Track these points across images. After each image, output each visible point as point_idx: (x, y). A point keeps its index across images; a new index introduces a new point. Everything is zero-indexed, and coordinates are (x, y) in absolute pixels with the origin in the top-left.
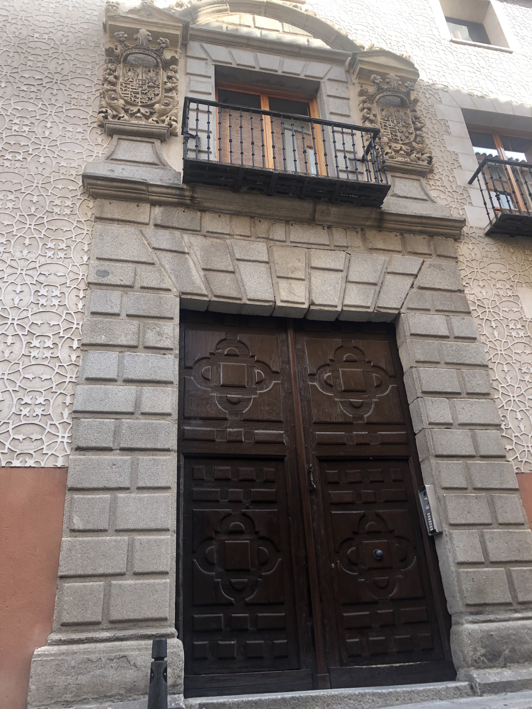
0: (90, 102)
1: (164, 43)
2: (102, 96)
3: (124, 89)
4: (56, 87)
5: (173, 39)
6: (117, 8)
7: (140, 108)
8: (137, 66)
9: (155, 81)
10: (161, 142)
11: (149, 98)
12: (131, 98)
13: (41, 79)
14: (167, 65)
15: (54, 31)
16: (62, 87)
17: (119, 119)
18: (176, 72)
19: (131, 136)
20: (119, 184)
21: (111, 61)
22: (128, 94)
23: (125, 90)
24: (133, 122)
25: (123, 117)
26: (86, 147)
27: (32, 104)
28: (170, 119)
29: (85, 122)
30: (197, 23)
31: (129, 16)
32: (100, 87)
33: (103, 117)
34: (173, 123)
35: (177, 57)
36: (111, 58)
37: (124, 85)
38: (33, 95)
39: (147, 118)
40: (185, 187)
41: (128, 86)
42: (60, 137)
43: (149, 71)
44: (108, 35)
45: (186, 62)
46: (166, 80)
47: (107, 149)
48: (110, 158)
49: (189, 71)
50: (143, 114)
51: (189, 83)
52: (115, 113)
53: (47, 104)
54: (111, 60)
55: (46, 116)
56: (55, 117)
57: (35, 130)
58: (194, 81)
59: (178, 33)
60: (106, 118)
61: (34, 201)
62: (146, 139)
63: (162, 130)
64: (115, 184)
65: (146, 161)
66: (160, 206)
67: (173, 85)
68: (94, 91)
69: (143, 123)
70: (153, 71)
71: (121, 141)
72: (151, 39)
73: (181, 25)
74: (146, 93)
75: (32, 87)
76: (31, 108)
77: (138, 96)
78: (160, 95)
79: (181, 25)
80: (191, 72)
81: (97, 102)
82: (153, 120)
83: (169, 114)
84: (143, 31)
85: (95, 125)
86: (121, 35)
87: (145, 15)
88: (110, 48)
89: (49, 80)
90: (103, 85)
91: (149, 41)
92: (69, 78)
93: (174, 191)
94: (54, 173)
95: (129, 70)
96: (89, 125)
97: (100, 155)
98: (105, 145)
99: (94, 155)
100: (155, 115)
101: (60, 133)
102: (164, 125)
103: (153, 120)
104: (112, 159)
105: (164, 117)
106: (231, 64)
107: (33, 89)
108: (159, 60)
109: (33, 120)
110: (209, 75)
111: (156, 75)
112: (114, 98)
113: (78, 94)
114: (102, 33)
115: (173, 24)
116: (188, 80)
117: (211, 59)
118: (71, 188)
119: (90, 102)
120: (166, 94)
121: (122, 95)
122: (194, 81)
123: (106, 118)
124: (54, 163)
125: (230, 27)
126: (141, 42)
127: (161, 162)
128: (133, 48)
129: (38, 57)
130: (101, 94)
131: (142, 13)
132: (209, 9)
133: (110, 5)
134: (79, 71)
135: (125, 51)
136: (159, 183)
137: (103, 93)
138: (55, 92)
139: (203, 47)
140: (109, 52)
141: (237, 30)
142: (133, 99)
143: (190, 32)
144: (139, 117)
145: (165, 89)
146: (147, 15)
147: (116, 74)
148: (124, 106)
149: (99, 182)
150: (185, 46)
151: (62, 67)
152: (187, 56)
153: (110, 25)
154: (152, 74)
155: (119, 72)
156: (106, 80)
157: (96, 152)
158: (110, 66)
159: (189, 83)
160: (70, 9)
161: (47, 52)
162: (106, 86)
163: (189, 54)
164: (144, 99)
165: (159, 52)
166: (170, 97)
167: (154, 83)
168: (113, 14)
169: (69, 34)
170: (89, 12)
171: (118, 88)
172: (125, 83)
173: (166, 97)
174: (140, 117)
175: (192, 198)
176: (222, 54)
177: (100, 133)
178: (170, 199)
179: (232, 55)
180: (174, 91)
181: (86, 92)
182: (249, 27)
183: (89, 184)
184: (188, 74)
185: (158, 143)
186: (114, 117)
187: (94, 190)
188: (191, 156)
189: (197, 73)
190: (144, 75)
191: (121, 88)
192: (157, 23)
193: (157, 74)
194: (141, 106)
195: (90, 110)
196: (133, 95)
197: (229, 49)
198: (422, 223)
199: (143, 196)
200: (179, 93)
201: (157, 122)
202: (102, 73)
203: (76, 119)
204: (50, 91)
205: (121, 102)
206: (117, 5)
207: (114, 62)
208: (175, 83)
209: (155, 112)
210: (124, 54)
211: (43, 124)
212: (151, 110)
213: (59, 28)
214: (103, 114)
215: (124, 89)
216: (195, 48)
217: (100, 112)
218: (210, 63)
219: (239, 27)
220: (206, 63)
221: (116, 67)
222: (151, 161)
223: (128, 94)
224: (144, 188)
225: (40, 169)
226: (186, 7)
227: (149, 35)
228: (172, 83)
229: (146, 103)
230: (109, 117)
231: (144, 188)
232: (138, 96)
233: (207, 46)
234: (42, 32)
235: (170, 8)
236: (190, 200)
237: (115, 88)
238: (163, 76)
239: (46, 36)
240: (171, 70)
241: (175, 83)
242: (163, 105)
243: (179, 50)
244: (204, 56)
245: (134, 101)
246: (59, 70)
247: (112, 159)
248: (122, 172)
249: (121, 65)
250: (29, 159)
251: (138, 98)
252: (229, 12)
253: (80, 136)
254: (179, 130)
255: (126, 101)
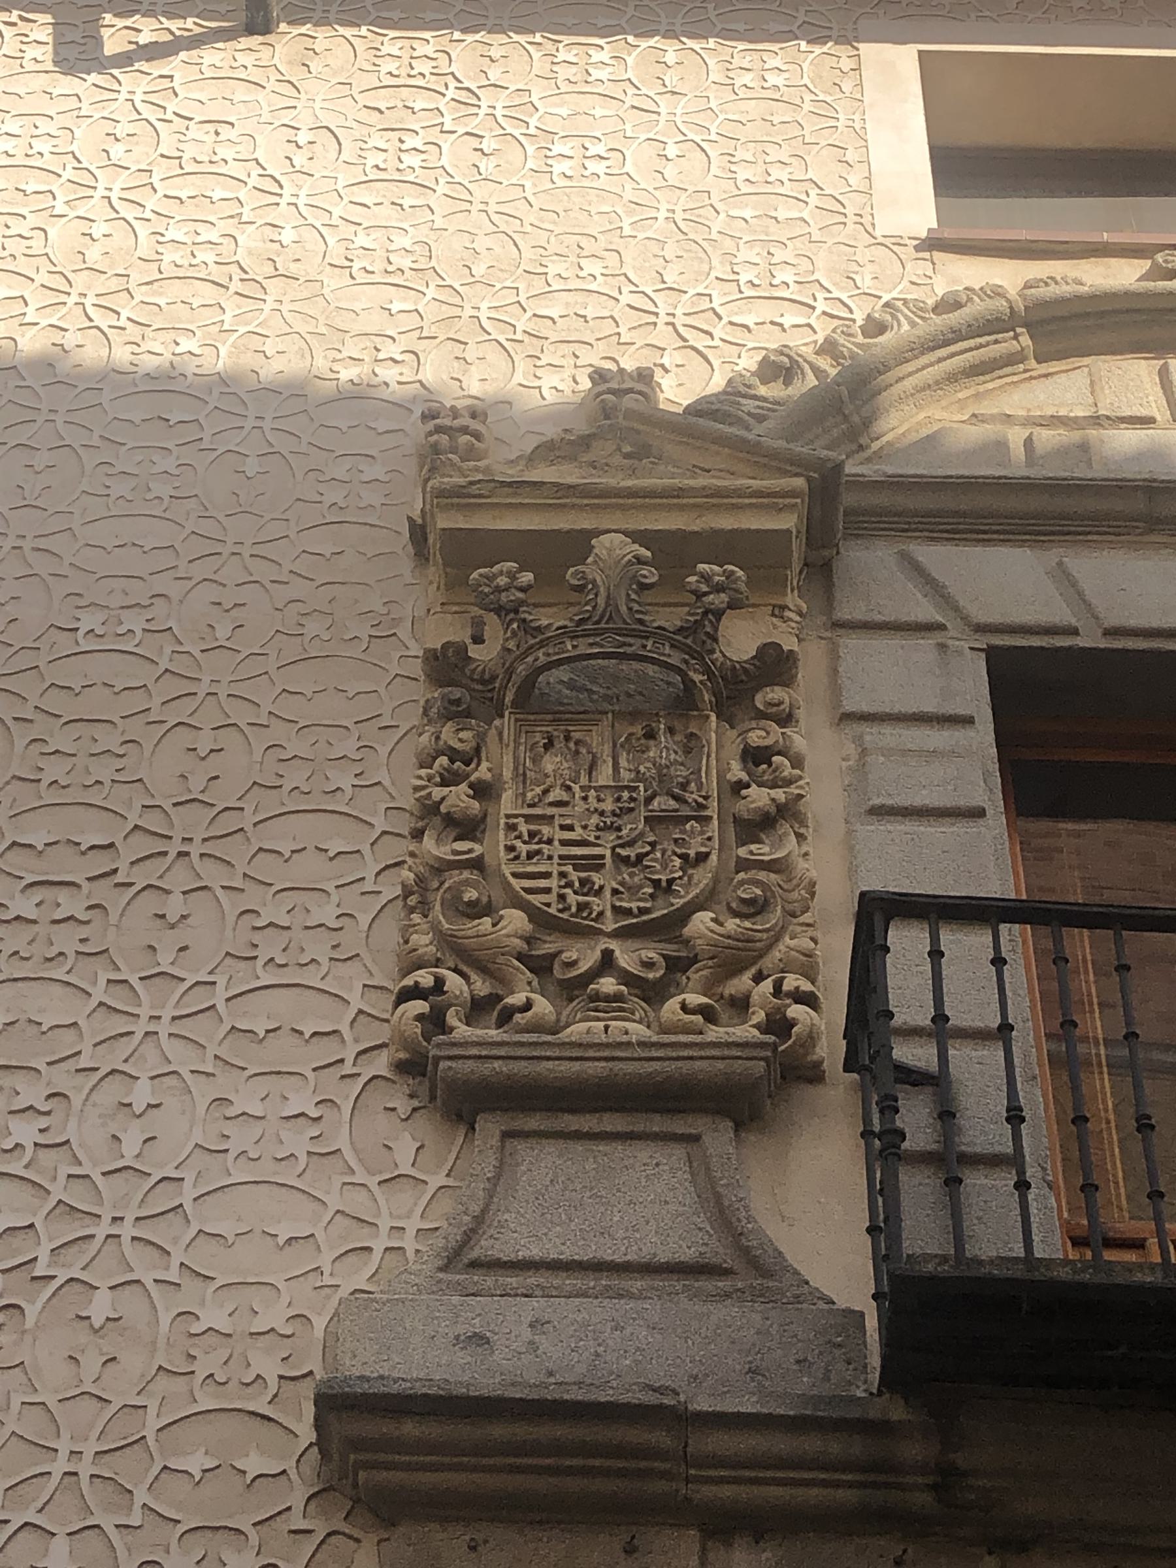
0: (352, 941)
1: (719, 589)
2: (412, 900)
3: (523, 849)
4: (179, 878)
5: (759, 556)
6: (477, 436)
7: (613, 945)
8: (588, 717)
9: (684, 786)
10: (738, 1126)
11: (656, 883)
12: (562, 897)
13: (111, 845)
14: (745, 688)
15: (175, 590)
16: (212, 874)
17: (506, 1017)
18: (786, 719)
19: (572, 1111)
20: (522, 1431)
21: (454, 712)
22: (546, 875)
23: (530, 856)
24: (576, 1031)
25: (528, 1006)
26: (334, 1202)
27: (57, 989)
28: (777, 990)
29: (326, 1051)
30: (875, 446)
31: (534, 476)
32: (398, 848)
33: (420, 1018)
34: (796, 1011)
35: (789, 643)
36: (457, 693)
37: (524, 828)
38: (67, 940)
39: (653, 993)
40: (898, 1412)
41: (546, 830)
42: (199, 1157)
43: (651, 735)
44: (434, 572)
45: (834, 655)
46: (737, 772)
47: (446, 1204)
48: (465, 1259)
49: (854, 702)
50: (627, 978)
51: (861, 768)
52: (482, 987)
53: (134, 981)
54: (458, 702)
55: (125, 1047)
56: (172, 1048)
57: (71, 1132)
58: (887, 752)
59: (787, 522)
60: (435, 1022)
61: (172, 918)
62: (657, 1123)
63: (739, 1066)
64: (499, 1431)
65: (663, 1257)
66: (758, 1536)
67: (780, 794)
68: (370, 876)
69: (638, 1031)
70: (671, 730)
71: (520, 1146)
72: (650, 575)
73: (800, 483)
74: (640, 857)
75: (63, 895)
76: (53, 1006)
77: (597, 879)
78: (714, 857)
79: (800, 483)
80: (865, 708)
81: (389, 935)
82: (684, 1007)
83: (767, 963)
84: (613, 545)
85: (381, 1064)
86: (502, 581)
87: (617, 460)
88: (445, 646)
89: (143, 845)
90: (417, 835)
91: (644, 587)
92: (247, 820)
93: (835, 1447)
94: (163, 1381)
95: (549, 746)
96: (348, 1069)
97: (409, 1243)
98: (438, 1179)
99: (378, 1246)
100: (696, 975)
101: (197, 1137)
102: (746, 1032)
103: (684, 1007)
104: (474, 1265)
105: (744, 981)
106: (1075, 632)
107: (70, 904)
108: (697, 678)
109: (61, 1079)
110: (961, 711)
111: (688, 751)
112: (471, 904)
113: (290, 899)
114: (405, 566)
115: (756, 484)
116: (851, 749)
117: (965, 619)
118: (254, 1464)
119: (352, 941)
120: (742, 852)
121: (517, 884)
122: (887, 752)
123: (435, 1022)
124: (165, 1319)
125: (1047, 438)
126: (601, 601)
127: (745, 1252)
128: (565, 633)
129: (98, 731)
130: (407, 893)
131: (601, 450)
132: (932, 367)
133: (439, 430)
134: (295, 777)
135: (526, 654)
136: (748, 1405)
137: (420, 880)
138: (174, 906)
139: (918, 571)
140: (445, 665)
141: (1084, 447)
142: (573, 899)
143: (848, 499)
144: (608, 999)
145: (736, 820)
146: (627, 456)
147: (483, 772)
148: (529, 940)
149: (410, 1429)
150: (821, 572)
151: (214, 765)
152: (838, 625)
153: (449, 534)
154: (664, 750)
155: (498, 762)
156: (430, 809)
157: (385, 1224)
158: (449, 734)
159: (861, 768)
160: (252, 466)
161: (137, 701)
162: (433, 847)
163: (844, 612)
164: (633, 890)
165: (699, 635)
166: (771, 866)
167: (676, 798)
168: (462, 481)
169: (247, 594)
170: (340, 471)
171: (494, 846)
172: (528, 818)
173: (743, 865)
174: (618, 998)
175: (946, 1479)
176: (1015, 587)
177: (403, 1105)
178: (814, 1491)
179: (1074, 584)
180: (784, 827)
181: (330, 887)
182: (1147, 421)
183: (356, 1444)
184: (847, 717)
185: (718, 1138)
186: (477, 1009)
187: (383, 1475)
188: (924, 1237)
189: (897, 708)
190: (623, 763)
191: (510, 849)
192: (680, 492)
193: (691, 746)
194: (617, 934)
195: (352, 984)
196: (574, 876)
197: (1053, 555)
198: (619, 1451)
199: (661, 1486)
200: (809, 833)
201: (708, 1014)
202: (413, 776)
203: (285, 1040)
204: (150, 903)
205: (515, 921)
206: (474, 425)
207: (468, 714)
208: (788, 782)
209: (695, 960)
210: (521, 670)
211: (113, 1091)
212: (671, 949)
213: (199, 570)
214: (419, 1006)
215: (523, 849)
216: (876, 574)
217: (406, 995)
218: (963, 643)
219: (1093, 433)
220: (942, 647)
221: (481, 737)
222: (687, 1254)
223: (546, 875)
224: (661, 1438)
225: (91, 1363)
226: (812, 381)
227: (639, 560)
228: (774, 786)
229: (642, 911)
230: (452, 1019)
231: (661, 1438)
232: (597, 879)
233: (934, 556)
234: (116, 601)
235: (735, 391)
236: (934, 1487)
237: (478, 849)
238: (721, 749)
239: (135, 622)
240: (762, 715)
241: (788, 782)
242: (736, 914)
243: (792, 599)
244: (924, 610)
245: (581, 907)
246: (197, 784)
247: (474, 1265)
248: (533, 1346)
249: (507, 723)
250: (32, 1312)
251: (599, 892)
252: (1033, 363)
253: (298, 1141)
254: (831, 1049)
255: (536, 916)
